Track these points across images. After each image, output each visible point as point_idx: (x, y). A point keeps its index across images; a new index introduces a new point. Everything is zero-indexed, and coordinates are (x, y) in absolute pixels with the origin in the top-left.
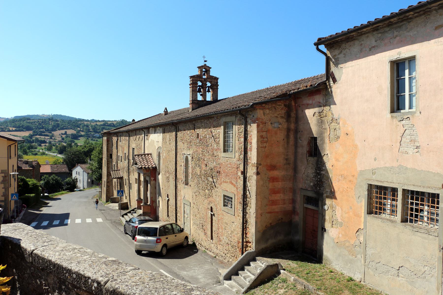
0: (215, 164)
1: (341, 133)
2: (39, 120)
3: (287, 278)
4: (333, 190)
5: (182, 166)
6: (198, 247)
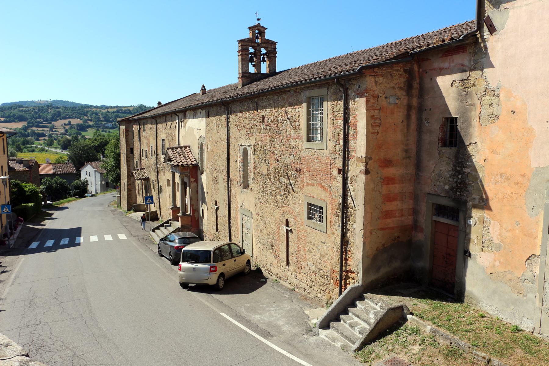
0: (292, 158)
1: (503, 111)
2: (34, 107)
3: (420, 327)
4: (484, 197)
5: (238, 162)
6: (266, 274)
